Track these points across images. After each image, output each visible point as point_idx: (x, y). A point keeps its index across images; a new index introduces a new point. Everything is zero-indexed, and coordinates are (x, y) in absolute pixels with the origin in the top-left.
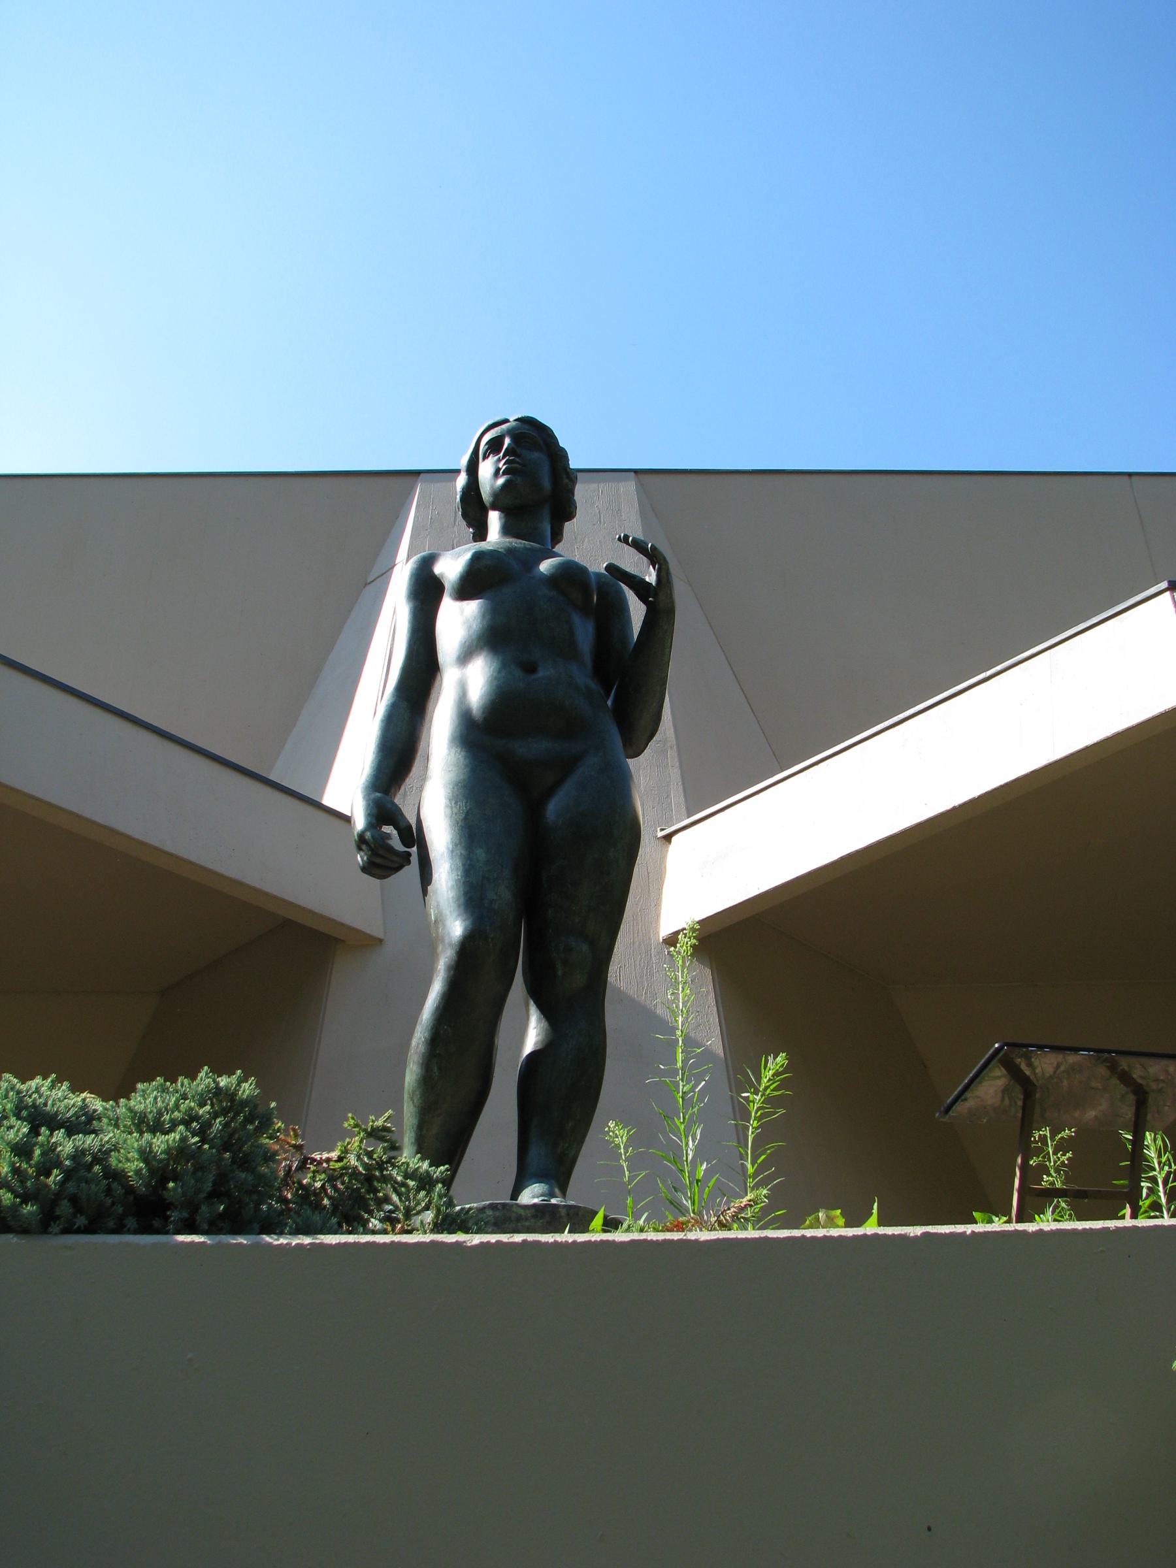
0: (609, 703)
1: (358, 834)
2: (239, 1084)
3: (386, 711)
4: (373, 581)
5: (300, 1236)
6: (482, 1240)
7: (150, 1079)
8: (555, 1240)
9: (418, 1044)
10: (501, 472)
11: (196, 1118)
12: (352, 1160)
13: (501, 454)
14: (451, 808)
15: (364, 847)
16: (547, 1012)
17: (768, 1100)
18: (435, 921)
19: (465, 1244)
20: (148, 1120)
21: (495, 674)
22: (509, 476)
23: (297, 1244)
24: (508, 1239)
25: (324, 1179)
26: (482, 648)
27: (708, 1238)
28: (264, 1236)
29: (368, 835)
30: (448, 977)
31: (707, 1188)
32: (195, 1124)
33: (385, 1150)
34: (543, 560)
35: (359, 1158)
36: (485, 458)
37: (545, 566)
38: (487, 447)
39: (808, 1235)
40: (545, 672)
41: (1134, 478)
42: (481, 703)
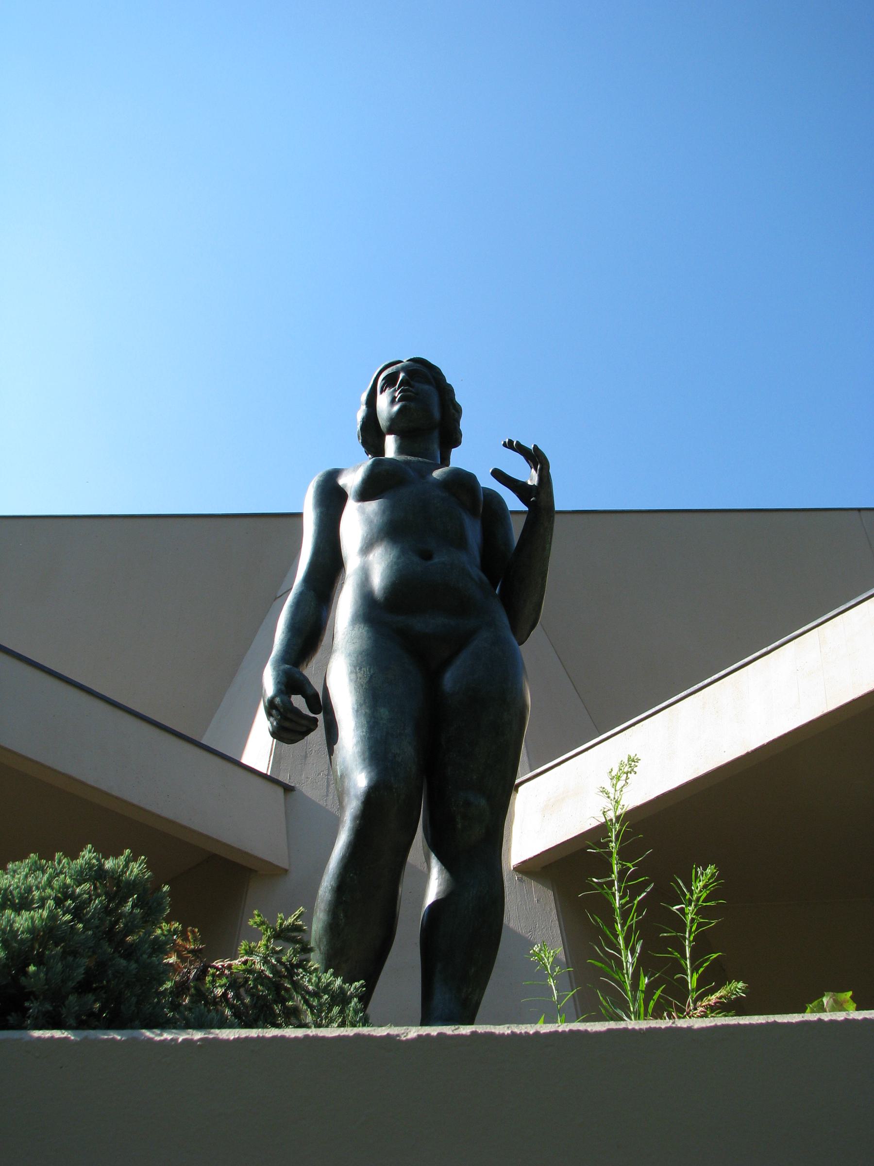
0: (497, 592)
1: (268, 700)
2: (126, 866)
3: (295, 598)
4: (281, 596)
5: (189, 1030)
6: (421, 1033)
7: (22, 857)
8: (512, 1032)
9: (325, 892)
10: (397, 400)
11: (73, 897)
12: (257, 962)
13: (397, 386)
14: (356, 673)
15: (274, 712)
16: (447, 863)
17: (700, 911)
18: (341, 776)
19: (398, 1038)
20: (13, 897)
21: (395, 560)
22: (404, 402)
23: (184, 1040)
24: (453, 1031)
25: (224, 985)
26: (382, 540)
27: (704, 1025)
28: (144, 1031)
29: (278, 700)
30: (353, 827)
31: (652, 1002)
32: (69, 902)
33: (295, 952)
34: (434, 470)
35: (265, 961)
36: (382, 391)
37: (437, 474)
38: (384, 381)
39: (826, 1019)
40: (440, 558)
41: (862, 512)
42: (383, 585)
